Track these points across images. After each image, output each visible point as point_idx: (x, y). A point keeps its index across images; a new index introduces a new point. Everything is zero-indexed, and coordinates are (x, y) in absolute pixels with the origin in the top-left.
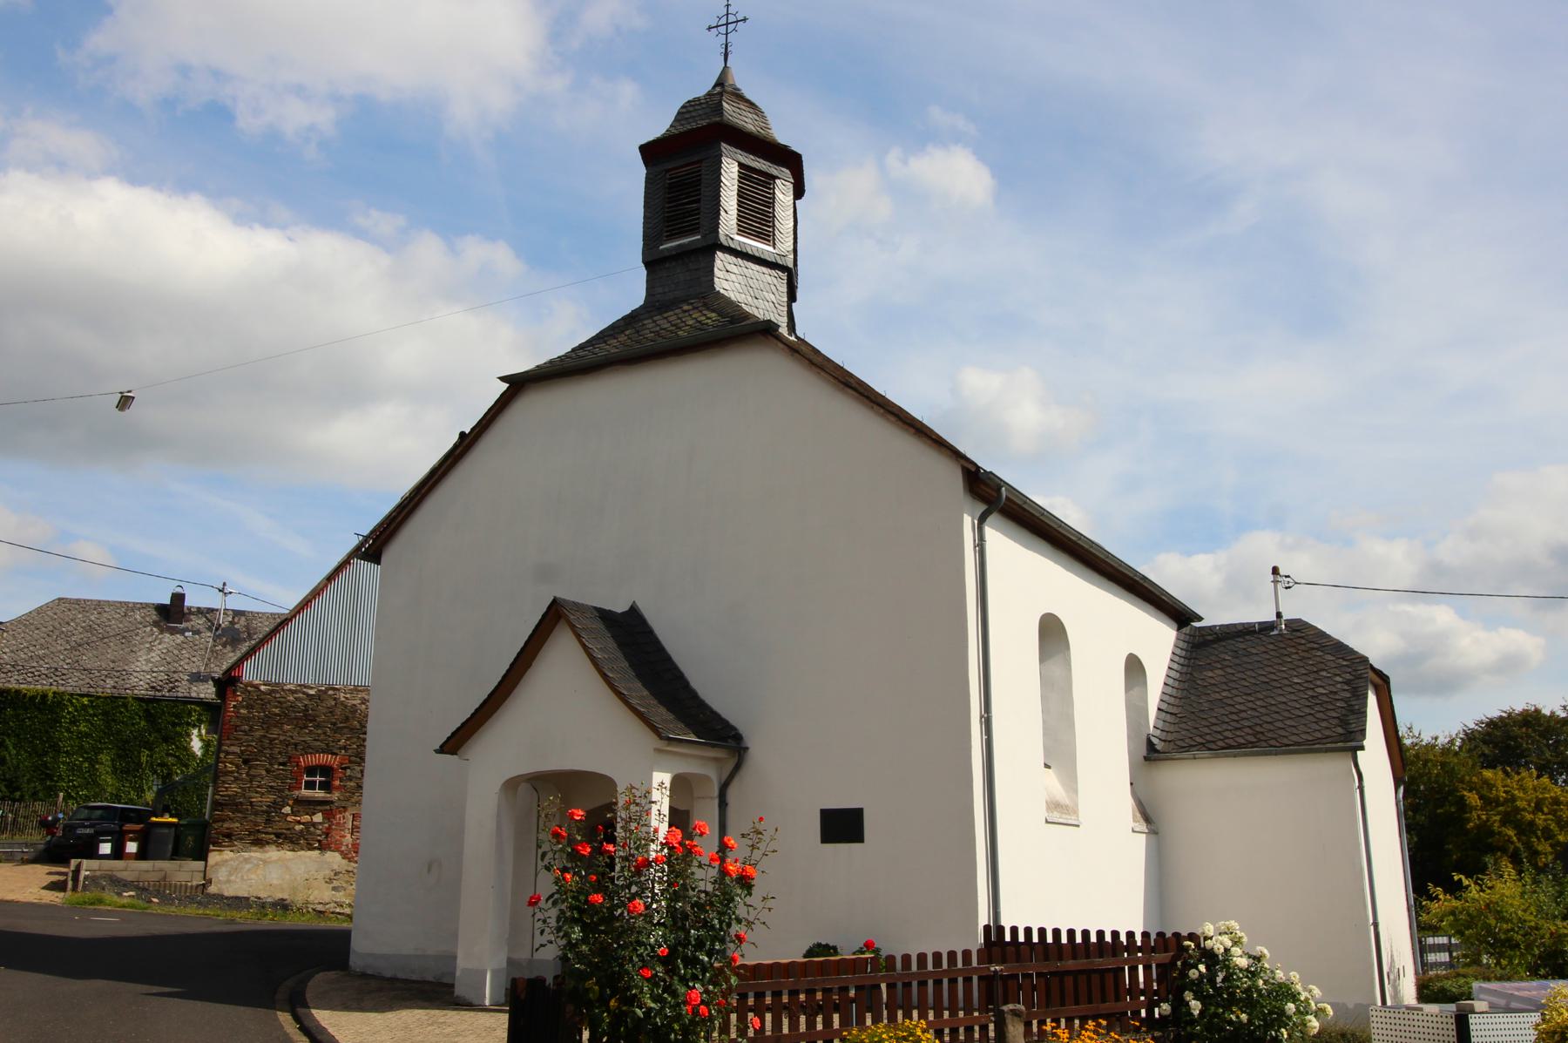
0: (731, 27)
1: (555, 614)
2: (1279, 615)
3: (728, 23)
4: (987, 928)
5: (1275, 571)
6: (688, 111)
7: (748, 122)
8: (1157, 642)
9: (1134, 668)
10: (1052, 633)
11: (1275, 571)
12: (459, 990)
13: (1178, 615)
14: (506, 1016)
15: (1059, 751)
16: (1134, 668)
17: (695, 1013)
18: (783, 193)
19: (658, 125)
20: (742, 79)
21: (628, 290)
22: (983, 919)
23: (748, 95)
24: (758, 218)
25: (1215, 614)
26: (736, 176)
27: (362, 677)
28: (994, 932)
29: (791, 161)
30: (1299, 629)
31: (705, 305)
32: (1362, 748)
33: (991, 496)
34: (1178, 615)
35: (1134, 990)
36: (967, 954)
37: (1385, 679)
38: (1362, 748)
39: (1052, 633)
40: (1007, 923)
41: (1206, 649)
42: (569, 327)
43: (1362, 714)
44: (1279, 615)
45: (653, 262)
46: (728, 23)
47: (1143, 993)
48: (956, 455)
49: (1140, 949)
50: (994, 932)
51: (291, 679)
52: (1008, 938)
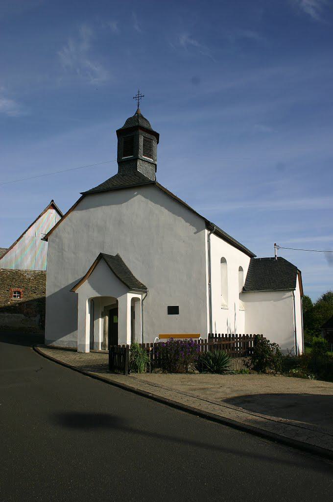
0: (137, 96)
1: (101, 257)
2: (276, 256)
3: (139, 97)
4: (209, 334)
5: (275, 245)
6: (129, 121)
7: (146, 126)
8: (246, 261)
9: (241, 269)
10: (223, 260)
11: (275, 245)
12: (79, 350)
13: (251, 255)
14: (108, 355)
15: (225, 292)
16: (241, 269)
17: (266, 361)
18: (154, 143)
19: (121, 124)
20: (142, 112)
21: (111, 169)
22: (208, 332)
23: (144, 117)
24: (149, 152)
25: (259, 255)
26: (142, 140)
27: (44, 269)
28: (211, 336)
29: (157, 135)
30: (280, 259)
31: (135, 175)
32: (295, 290)
33: (209, 226)
34: (251, 255)
35: (237, 348)
36: (206, 340)
37: (300, 272)
38: (295, 290)
39: (223, 260)
40: (214, 332)
41: (256, 264)
42: (163, 214)
43: (296, 279)
44: (276, 256)
45: (120, 162)
46: (139, 97)
47: (239, 348)
48: (204, 218)
49: (238, 338)
50: (211, 336)
51: (9, 268)
52: (214, 336)
